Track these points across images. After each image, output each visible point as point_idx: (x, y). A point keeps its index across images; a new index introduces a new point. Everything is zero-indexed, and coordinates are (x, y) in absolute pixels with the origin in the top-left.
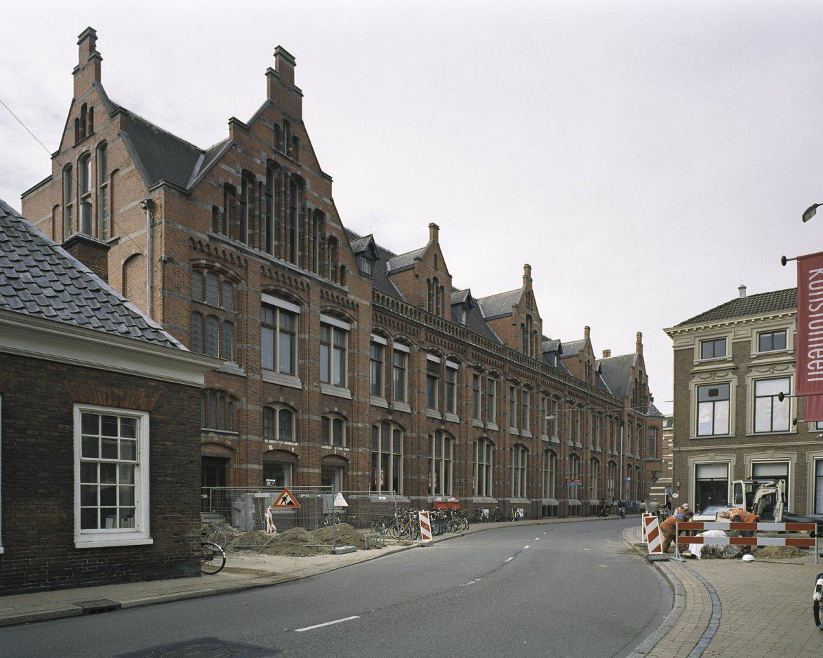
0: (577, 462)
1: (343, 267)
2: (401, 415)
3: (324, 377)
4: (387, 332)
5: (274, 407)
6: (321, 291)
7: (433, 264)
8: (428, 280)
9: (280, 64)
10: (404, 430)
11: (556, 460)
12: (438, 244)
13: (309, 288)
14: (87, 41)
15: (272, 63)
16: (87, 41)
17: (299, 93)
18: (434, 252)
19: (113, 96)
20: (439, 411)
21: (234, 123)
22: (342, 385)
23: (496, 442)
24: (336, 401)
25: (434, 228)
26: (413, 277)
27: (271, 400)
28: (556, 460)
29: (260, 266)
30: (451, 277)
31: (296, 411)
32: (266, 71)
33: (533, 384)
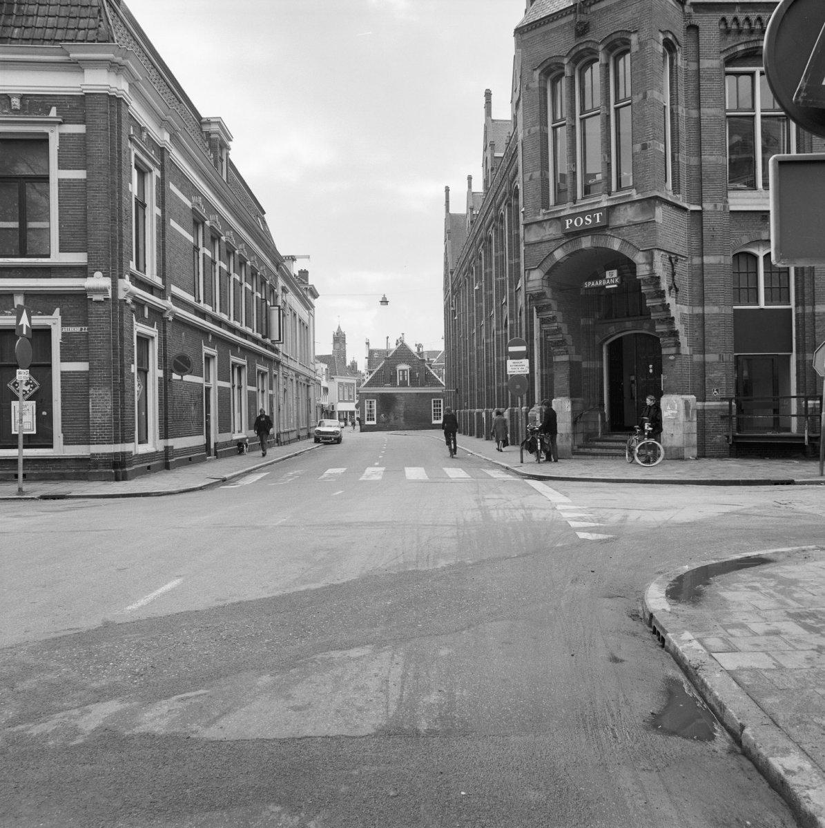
5: (754, 251)
27: (746, 240)
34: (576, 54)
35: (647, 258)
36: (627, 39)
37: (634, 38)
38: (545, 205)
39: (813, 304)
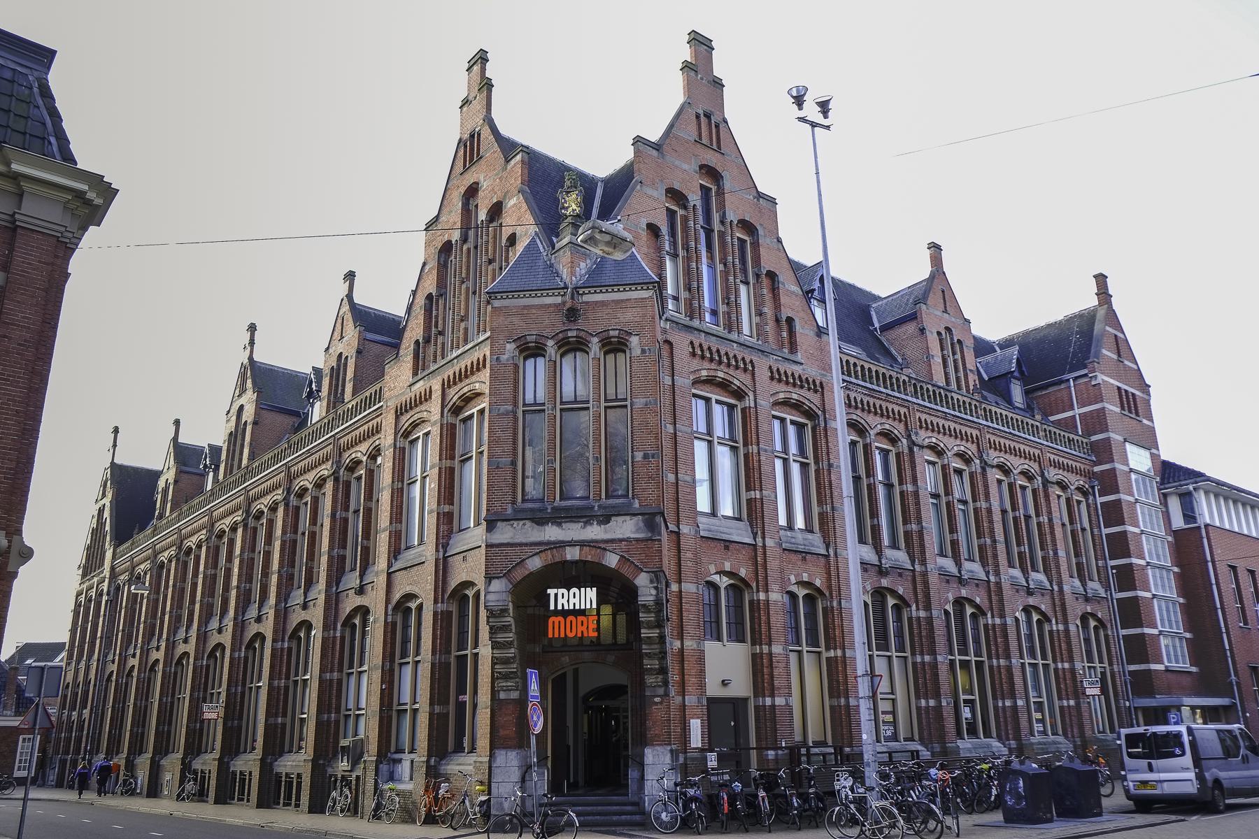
0: (1102, 633)
1: (790, 321)
2: (804, 559)
3: (703, 504)
4: (942, 445)
6: (692, 343)
7: (942, 306)
8: (939, 333)
9: (696, 54)
10: (984, 614)
11: (1106, 636)
12: (944, 273)
13: (753, 367)
14: (476, 68)
15: (686, 54)
16: (476, 68)
17: (718, 84)
18: (940, 287)
19: (504, 131)
20: (952, 557)
21: (638, 141)
22: (809, 529)
23: (1050, 614)
24: (727, 548)
25: (935, 248)
26: (917, 332)
28: (1106, 636)
29: (689, 341)
30: (968, 322)
31: (748, 585)
32: (680, 66)
33: (898, 430)
34: (563, 339)
35: (652, 582)
36: (628, 341)
37: (634, 341)
38: (514, 502)
39: (770, 645)
